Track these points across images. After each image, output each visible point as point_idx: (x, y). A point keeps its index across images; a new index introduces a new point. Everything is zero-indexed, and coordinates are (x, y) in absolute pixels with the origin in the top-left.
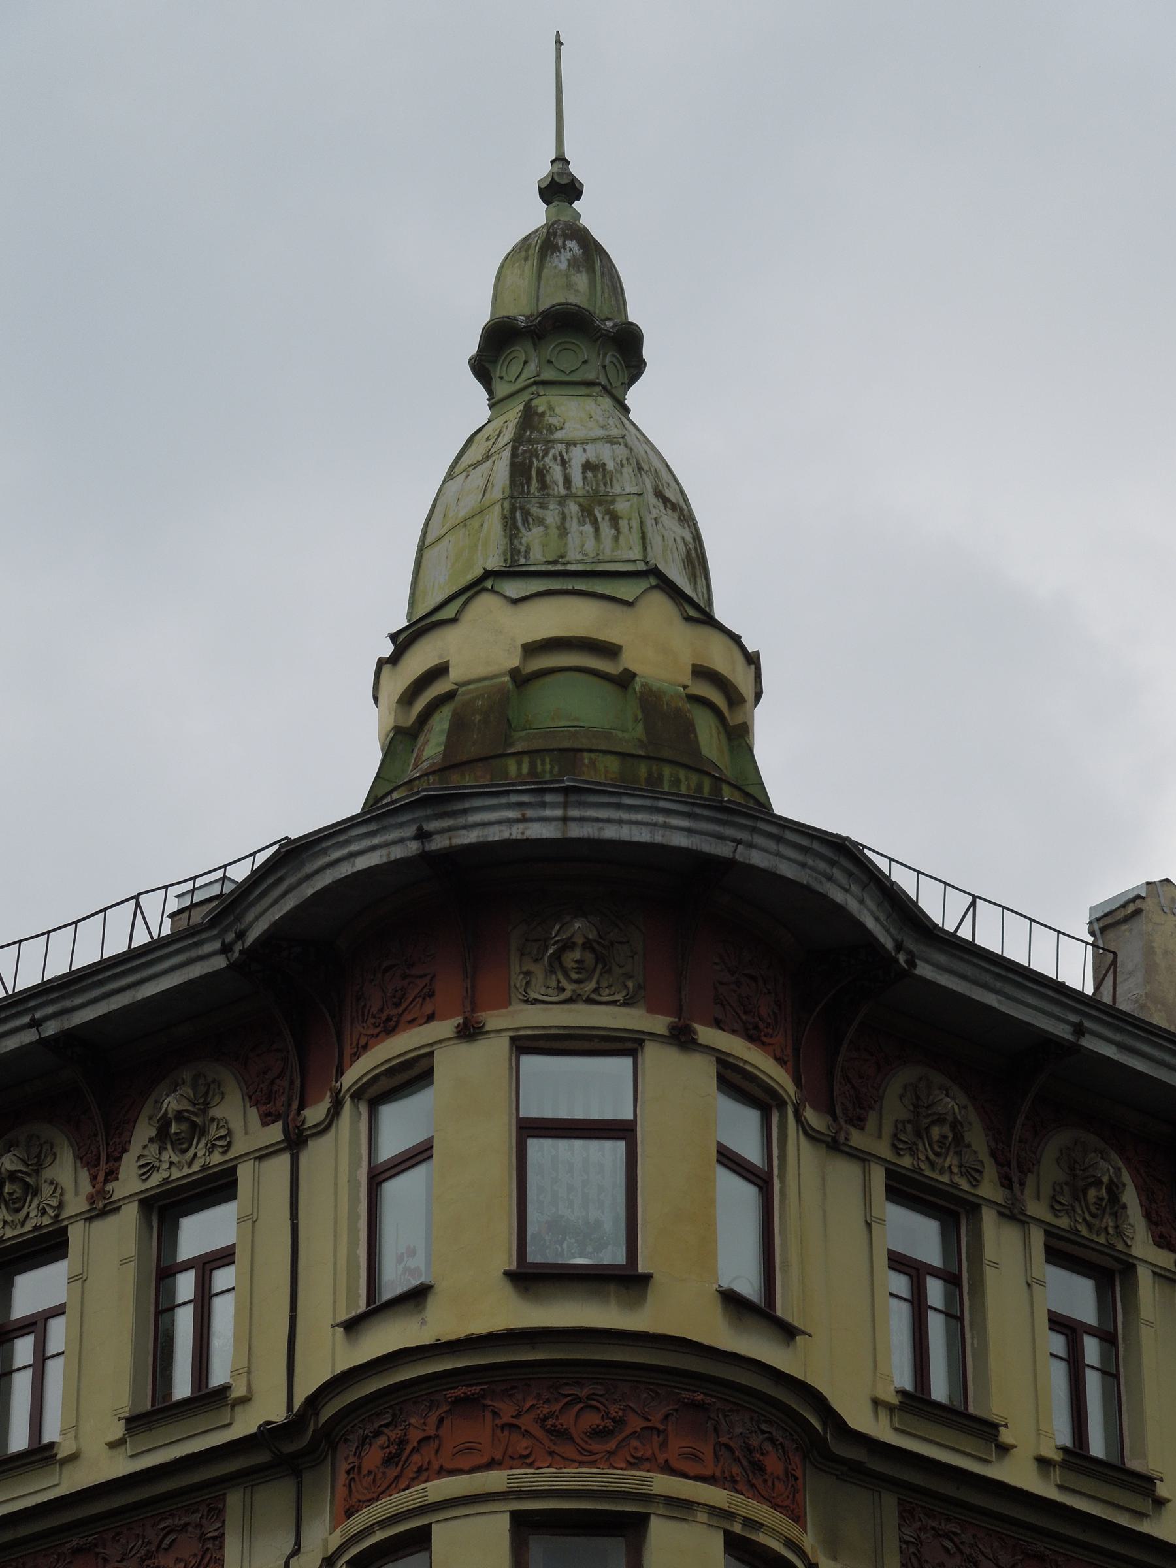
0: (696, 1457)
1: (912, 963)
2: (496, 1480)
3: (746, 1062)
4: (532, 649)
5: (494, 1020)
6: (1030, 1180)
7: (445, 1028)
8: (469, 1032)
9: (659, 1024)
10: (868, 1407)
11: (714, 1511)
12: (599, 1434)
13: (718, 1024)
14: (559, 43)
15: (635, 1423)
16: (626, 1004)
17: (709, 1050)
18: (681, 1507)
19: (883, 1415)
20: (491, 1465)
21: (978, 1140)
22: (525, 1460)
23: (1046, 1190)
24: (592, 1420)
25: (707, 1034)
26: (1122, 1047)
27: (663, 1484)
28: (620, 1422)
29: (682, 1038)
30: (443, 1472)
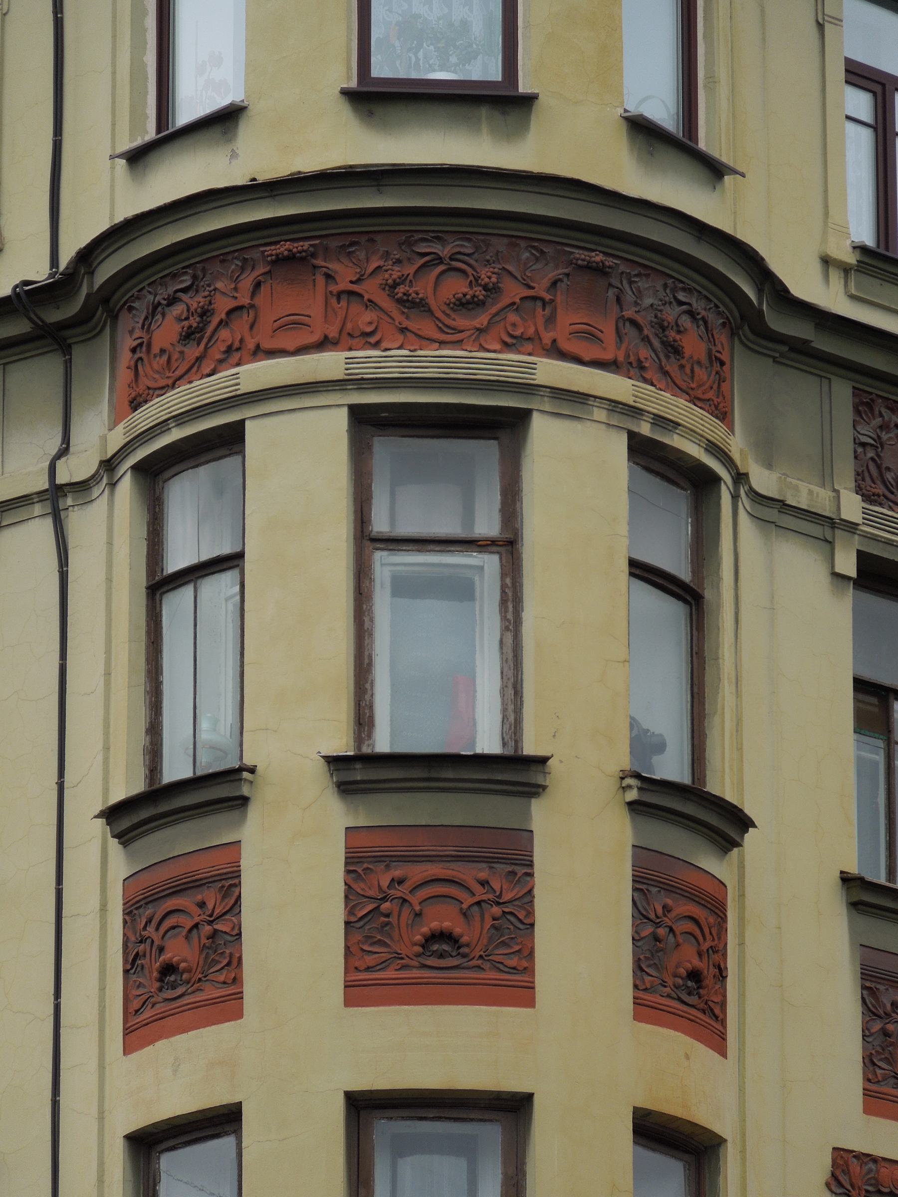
0: (591, 336)
3: (687, 702)
10: (816, 267)
11: (615, 406)
15: (513, 291)
19: (835, 276)
20: (324, 344)
24: (456, 286)
28: (492, 290)
30: (261, 352)
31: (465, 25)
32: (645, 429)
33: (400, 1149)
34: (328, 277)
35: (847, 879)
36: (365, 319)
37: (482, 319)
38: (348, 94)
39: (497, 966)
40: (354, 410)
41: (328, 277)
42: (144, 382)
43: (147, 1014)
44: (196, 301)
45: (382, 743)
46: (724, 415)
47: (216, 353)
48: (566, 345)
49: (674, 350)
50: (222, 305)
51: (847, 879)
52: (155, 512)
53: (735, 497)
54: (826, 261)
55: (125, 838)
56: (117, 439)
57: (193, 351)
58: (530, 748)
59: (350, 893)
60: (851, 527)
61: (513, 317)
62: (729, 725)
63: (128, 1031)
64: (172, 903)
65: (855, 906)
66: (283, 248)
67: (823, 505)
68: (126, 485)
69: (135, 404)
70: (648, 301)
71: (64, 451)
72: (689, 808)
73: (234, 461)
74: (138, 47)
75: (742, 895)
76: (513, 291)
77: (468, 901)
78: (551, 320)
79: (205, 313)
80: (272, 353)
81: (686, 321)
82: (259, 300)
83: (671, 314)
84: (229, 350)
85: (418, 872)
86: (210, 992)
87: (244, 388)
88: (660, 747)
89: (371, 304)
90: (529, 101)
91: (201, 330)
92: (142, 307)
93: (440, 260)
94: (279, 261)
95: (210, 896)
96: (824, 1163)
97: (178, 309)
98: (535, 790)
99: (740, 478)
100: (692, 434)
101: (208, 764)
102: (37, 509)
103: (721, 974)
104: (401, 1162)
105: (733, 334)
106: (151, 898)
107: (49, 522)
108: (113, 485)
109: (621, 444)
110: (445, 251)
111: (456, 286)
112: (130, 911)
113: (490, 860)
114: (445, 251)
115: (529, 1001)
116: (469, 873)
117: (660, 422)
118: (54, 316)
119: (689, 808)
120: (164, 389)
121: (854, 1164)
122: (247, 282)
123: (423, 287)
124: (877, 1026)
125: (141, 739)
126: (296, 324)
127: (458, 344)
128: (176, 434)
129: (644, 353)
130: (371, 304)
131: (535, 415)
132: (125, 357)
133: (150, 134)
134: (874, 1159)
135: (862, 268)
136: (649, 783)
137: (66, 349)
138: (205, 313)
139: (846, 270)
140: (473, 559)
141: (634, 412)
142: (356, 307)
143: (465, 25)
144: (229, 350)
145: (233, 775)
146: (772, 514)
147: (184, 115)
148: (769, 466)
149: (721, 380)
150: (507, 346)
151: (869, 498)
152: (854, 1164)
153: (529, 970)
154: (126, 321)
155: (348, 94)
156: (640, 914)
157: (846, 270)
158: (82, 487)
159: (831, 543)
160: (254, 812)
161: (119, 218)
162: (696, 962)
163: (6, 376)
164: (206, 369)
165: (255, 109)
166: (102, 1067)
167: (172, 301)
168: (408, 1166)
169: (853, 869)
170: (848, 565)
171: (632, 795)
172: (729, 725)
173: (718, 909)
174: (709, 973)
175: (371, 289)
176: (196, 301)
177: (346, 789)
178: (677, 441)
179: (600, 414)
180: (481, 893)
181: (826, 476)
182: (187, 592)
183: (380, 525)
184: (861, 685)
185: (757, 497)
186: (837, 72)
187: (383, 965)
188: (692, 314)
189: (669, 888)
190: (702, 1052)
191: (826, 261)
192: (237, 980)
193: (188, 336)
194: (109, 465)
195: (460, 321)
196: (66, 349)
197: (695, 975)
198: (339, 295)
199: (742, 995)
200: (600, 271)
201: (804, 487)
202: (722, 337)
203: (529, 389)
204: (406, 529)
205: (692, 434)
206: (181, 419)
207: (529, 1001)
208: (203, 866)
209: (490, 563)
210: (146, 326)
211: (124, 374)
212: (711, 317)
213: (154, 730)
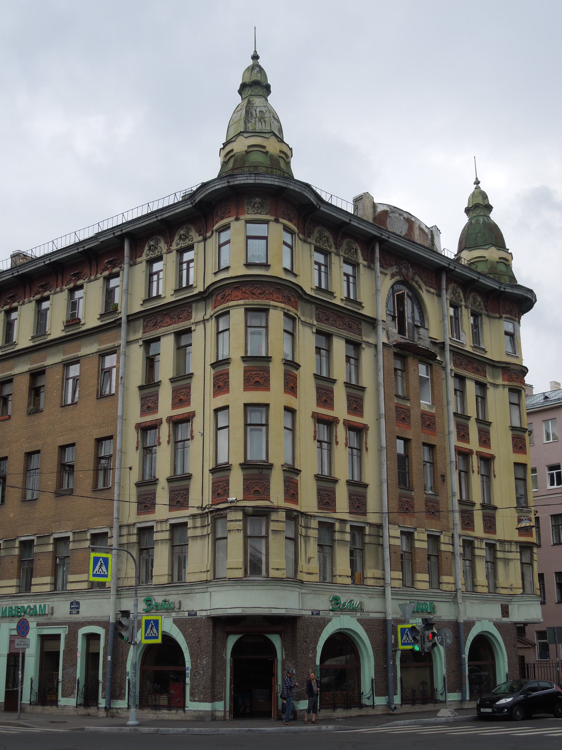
0: (278, 298)
1: (320, 207)
2: (242, 302)
4: (249, 147)
5: (242, 217)
6: (341, 248)
7: (232, 218)
8: (237, 219)
9: (272, 218)
11: (281, 308)
12: (154, 325)
13: (284, 218)
14: (255, 28)
16: (266, 214)
17: (282, 223)
18: (276, 307)
19: (313, 290)
20: (241, 299)
21: (331, 240)
22: (247, 298)
23: (344, 250)
24: (259, 291)
25: (281, 220)
26: (358, 223)
27: (272, 303)
28: (264, 292)
29: (277, 221)
30: (232, 300)
31: (261, 255)
32: (286, 311)
33: (251, 411)
34: (242, 290)
35: (314, 374)
36: (246, 296)
37: (263, 296)
38: (244, 265)
39: (265, 386)
40: (245, 308)
41: (242, 290)
42: (216, 305)
43: (216, 393)
44: (223, 293)
45: (249, 355)
46: (297, 309)
47: (226, 300)
48: (275, 299)
49: (290, 300)
50: (227, 294)
51: (314, 374)
52: (393, 660)
53: (299, 321)
54: (312, 288)
55: (213, 368)
56: (212, 313)
57: (223, 300)
58: (269, 356)
59: (244, 376)
60: (315, 325)
61: (267, 295)
62: (298, 353)
63: (214, 395)
64: (219, 377)
65: (315, 378)
66: (235, 286)
67: (311, 322)
68: (214, 319)
69: (215, 308)
70: (286, 293)
71: (205, 315)
72: (292, 364)
73: (228, 316)
74: (216, 258)
75: (299, 376)
76: (268, 292)
77: (261, 377)
78: (272, 296)
79: (224, 295)
80: (234, 300)
81: (292, 296)
82: (232, 293)
83: (289, 295)
84: (228, 300)
85: (254, 373)
86: (225, 389)
87: (230, 305)
88: (288, 356)
89: (248, 293)
90: (270, 265)
91: (224, 297)
92: (216, 294)
93: (257, 287)
94: (235, 288)
95: (225, 376)
96: (311, 414)
97: (221, 294)
98: (270, 361)
99: (299, 318)
100: (292, 312)
101: (225, 358)
102: (202, 323)
103: (296, 387)
104: (252, 413)
105: (298, 298)
106: (217, 377)
107: (203, 325)
108: (212, 319)
109: (282, 313)
110: (258, 286)
111: (259, 291)
112: (214, 378)
113: (264, 371)
114: (258, 286)
115: (269, 391)
116: (261, 373)
117: (288, 310)
118: (204, 296)
119: (292, 364)
120: (219, 306)
121: (315, 414)
122: (230, 291)
123: (255, 291)
124: (318, 395)
125: (216, 354)
126: (237, 296)
127: (259, 299)
128: (220, 312)
129: (286, 300)
130: (248, 293)
131: (270, 309)
132: (214, 301)
133: (217, 270)
134: (318, 413)
135: (316, 289)
136: (286, 360)
137: (206, 301)
138: (224, 295)
139: (314, 290)
140: (262, 329)
141: (284, 309)
142: (245, 294)
143: (261, 255)
144: (228, 300)
145: (228, 359)
146: (304, 324)
147: (222, 268)
148: (304, 317)
149: (296, 304)
150: (266, 299)
151: (317, 321)
152: (315, 414)
153: (269, 386)
154: (214, 296)
155: (244, 265)
156: (285, 379)
157: (314, 290)
158: (208, 320)
159: (312, 328)
160: (231, 365)
161: (213, 281)
162: (293, 385)
163: (207, 306)
164: (157, 328)
165: (232, 266)
166: (210, 400)
167: (220, 293)
168: (253, 414)
169: (315, 373)
170: (314, 331)
171: (284, 362)
172: (298, 353)
173: (296, 378)
174: (295, 387)
175: (247, 291)
176: (223, 293)
177: (244, 361)
178: (290, 313)
179: (279, 309)
180: (262, 376)
181: (311, 318)
182: (222, 334)
183: (249, 324)
184: (316, 347)
185: (301, 320)
186: (313, 263)
187: (249, 386)
188: (293, 295)
189: (289, 375)
190: (294, 398)
191: (312, 288)
192: (229, 388)
193: (222, 298)
194: (211, 316)
195: (260, 296)
196: (206, 301)
197: (293, 387)
198: (243, 292)
199: (299, 391)
200: (279, 289)
201: (308, 320)
202: (297, 299)
203: (270, 305)
204: (253, 325)
205: (292, 312)
206: (221, 310)
207: (269, 391)
208: (224, 372)
209: (264, 330)
210: (216, 297)
211: (213, 304)
212: (295, 296)
213: (217, 353)
